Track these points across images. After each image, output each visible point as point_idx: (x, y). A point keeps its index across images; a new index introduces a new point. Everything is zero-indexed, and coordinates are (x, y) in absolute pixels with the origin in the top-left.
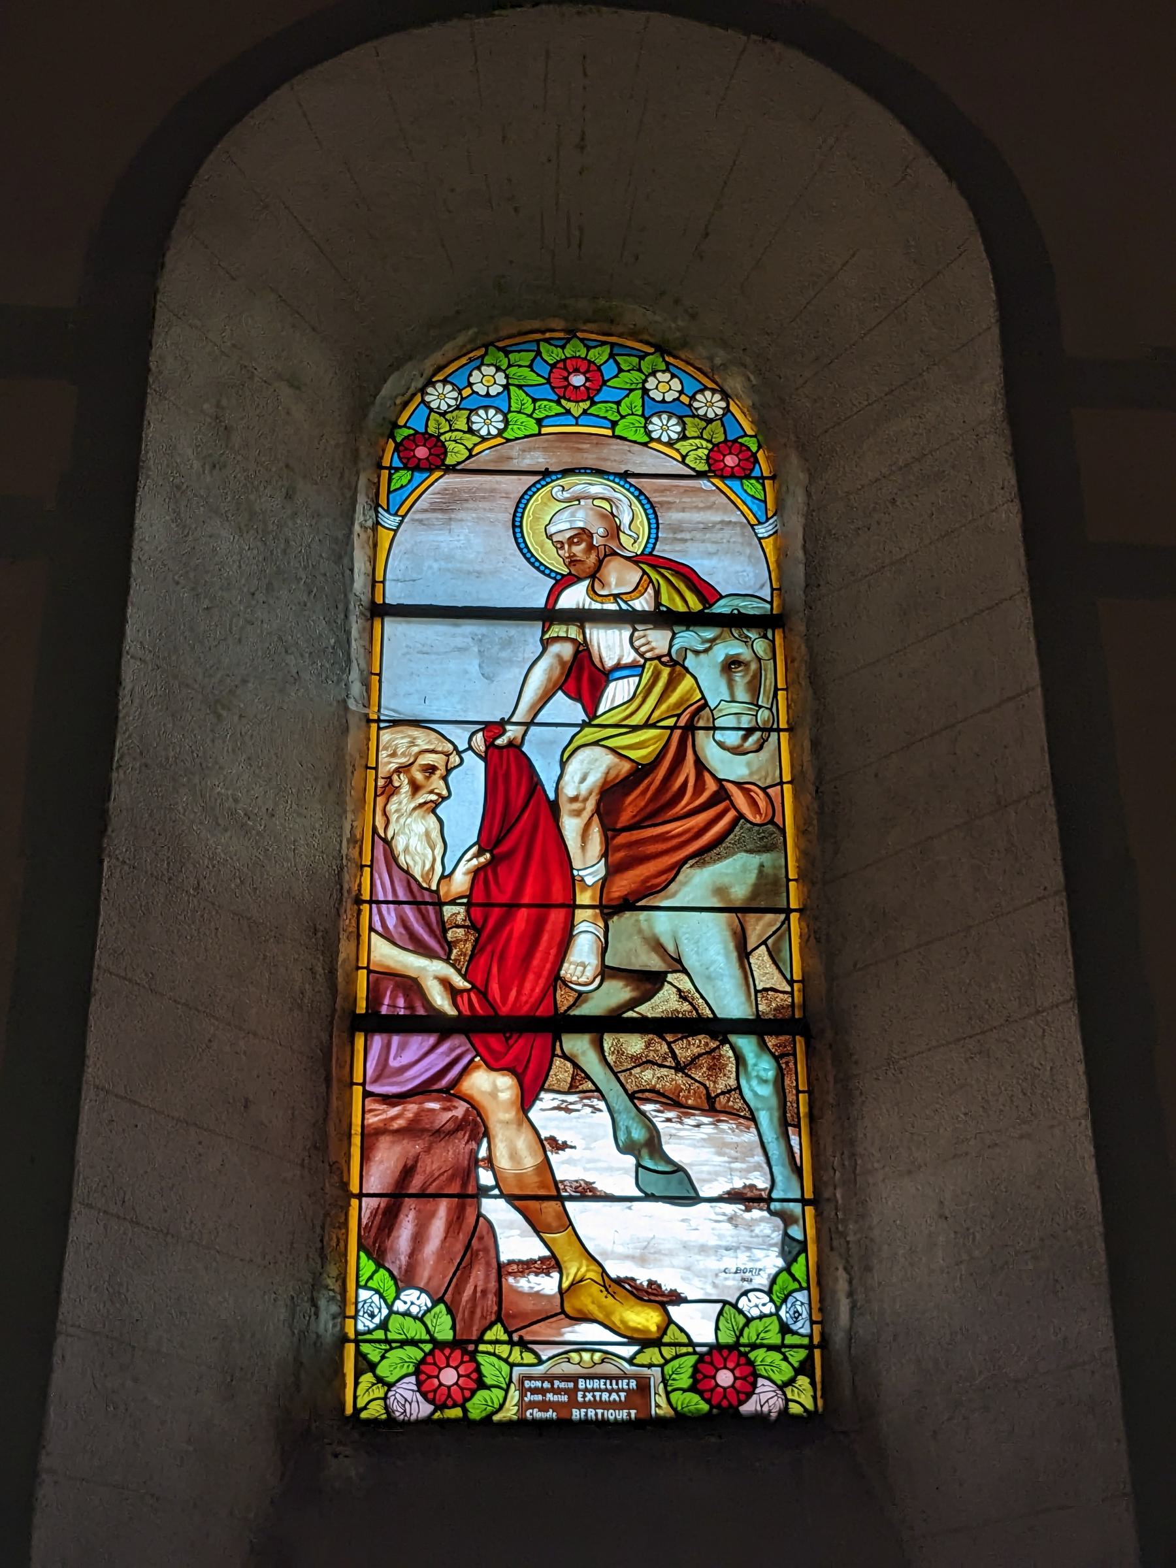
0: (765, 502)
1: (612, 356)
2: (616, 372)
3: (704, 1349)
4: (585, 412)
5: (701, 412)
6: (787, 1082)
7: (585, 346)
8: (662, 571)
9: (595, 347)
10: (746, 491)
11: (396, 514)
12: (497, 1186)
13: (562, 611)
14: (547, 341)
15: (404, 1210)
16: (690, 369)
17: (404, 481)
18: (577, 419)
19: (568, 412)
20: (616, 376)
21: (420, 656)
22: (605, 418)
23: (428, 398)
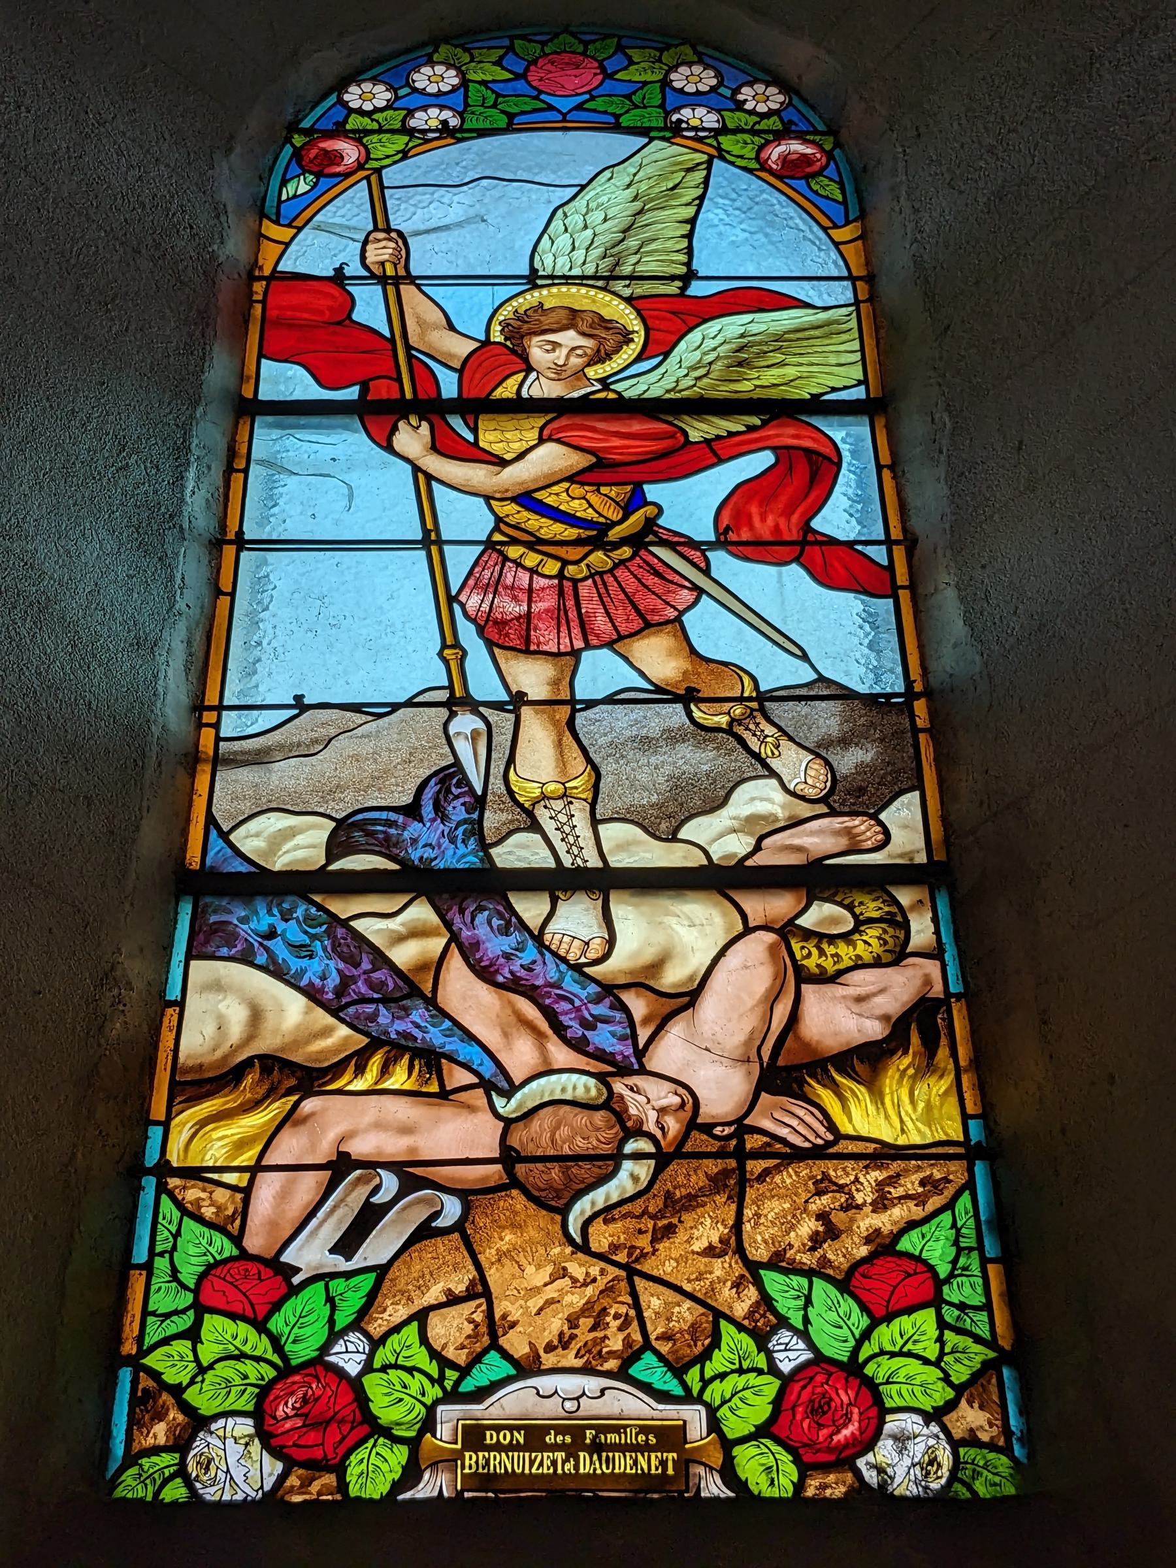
0: (844, 203)
1: (620, 49)
2: (626, 63)
3: (728, 1131)
4: (579, 107)
5: (749, 106)
6: (477, 570)
7: (581, 41)
8: (571, 533)
9: (594, 41)
10: (816, 192)
11: (289, 226)
12: (290, 1465)
13: (515, 1368)
14: (523, 37)
15: (132, 1280)
16: (731, 60)
17: (303, 188)
18: (564, 115)
19: (551, 108)
20: (625, 68)
21: (882, 986)
22: (605, 112)
23: (346, 97)
